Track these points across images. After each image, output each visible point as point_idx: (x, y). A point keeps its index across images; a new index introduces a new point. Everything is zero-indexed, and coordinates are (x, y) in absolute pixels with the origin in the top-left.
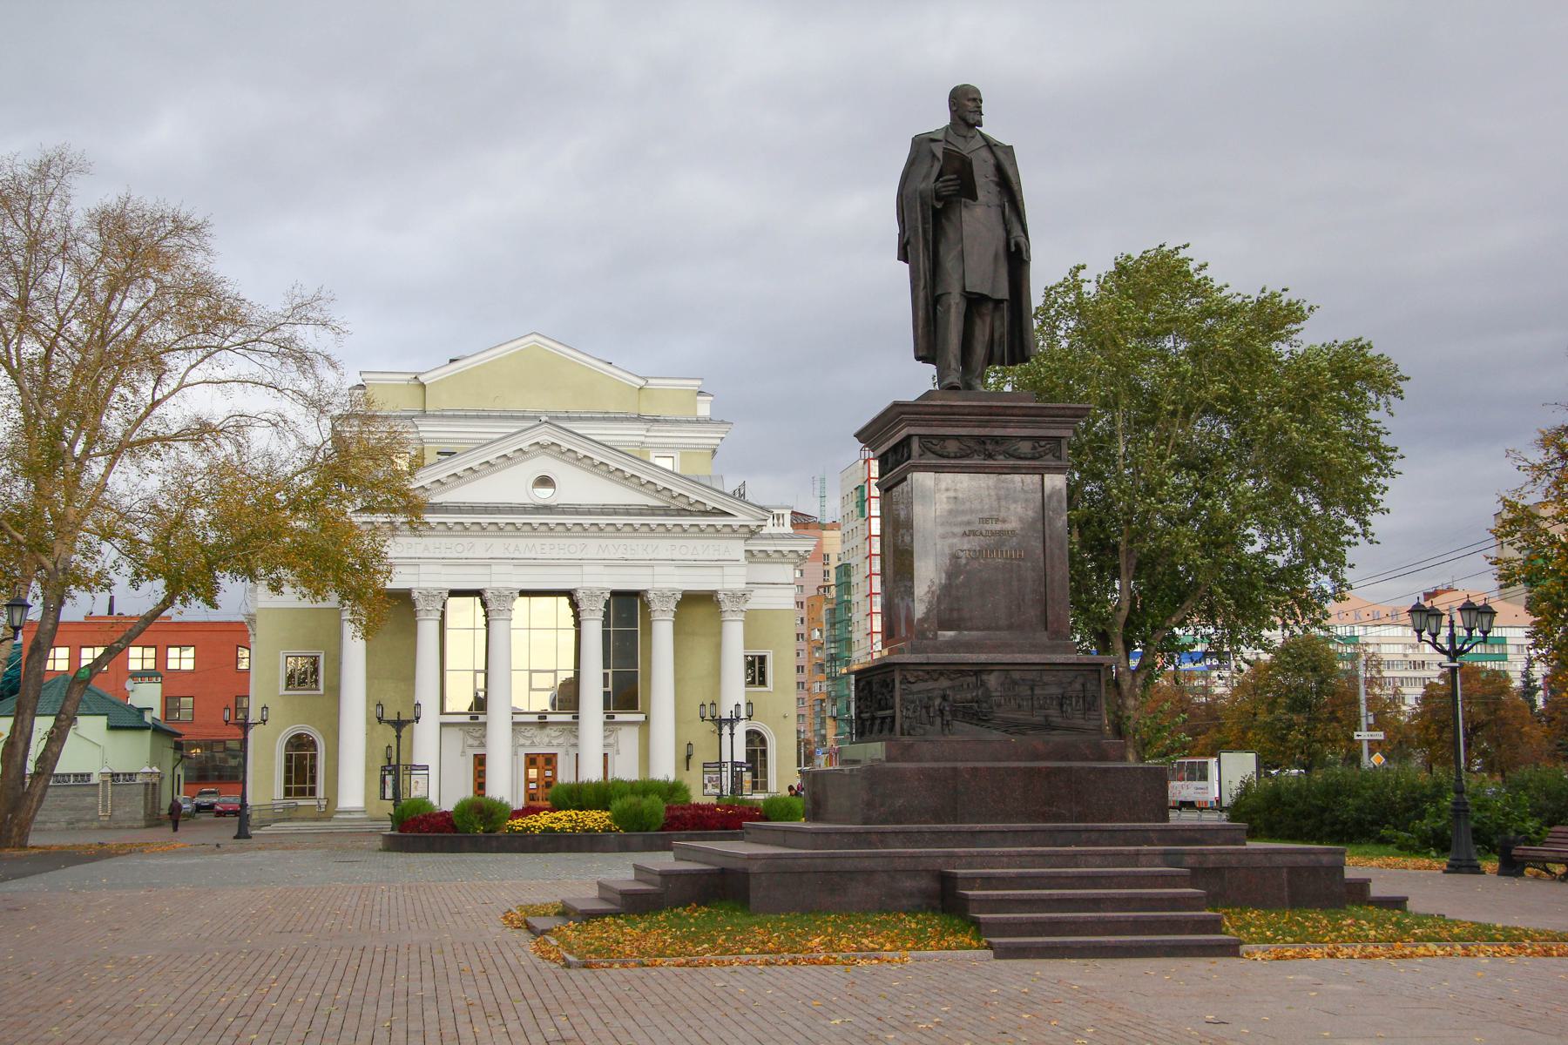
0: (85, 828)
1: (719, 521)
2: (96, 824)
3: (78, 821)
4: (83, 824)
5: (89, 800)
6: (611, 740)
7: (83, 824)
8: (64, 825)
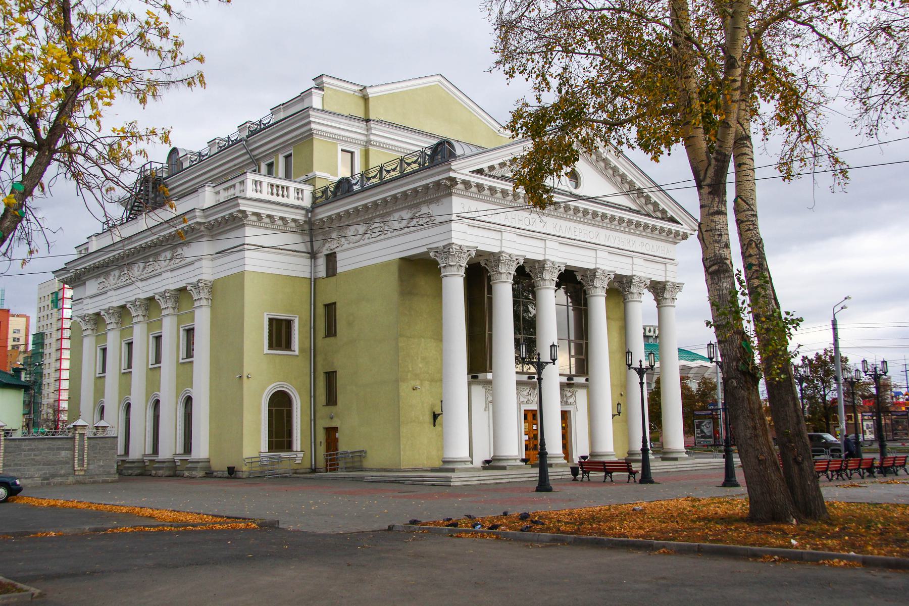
0: (61, 484)
1: (667, 225)
2: (71, 479)
3: (53, 476)
4: (58, 480)
5: (63, 453)
6: (571, 400)
7: (58, 480)
8: (38, 480)
